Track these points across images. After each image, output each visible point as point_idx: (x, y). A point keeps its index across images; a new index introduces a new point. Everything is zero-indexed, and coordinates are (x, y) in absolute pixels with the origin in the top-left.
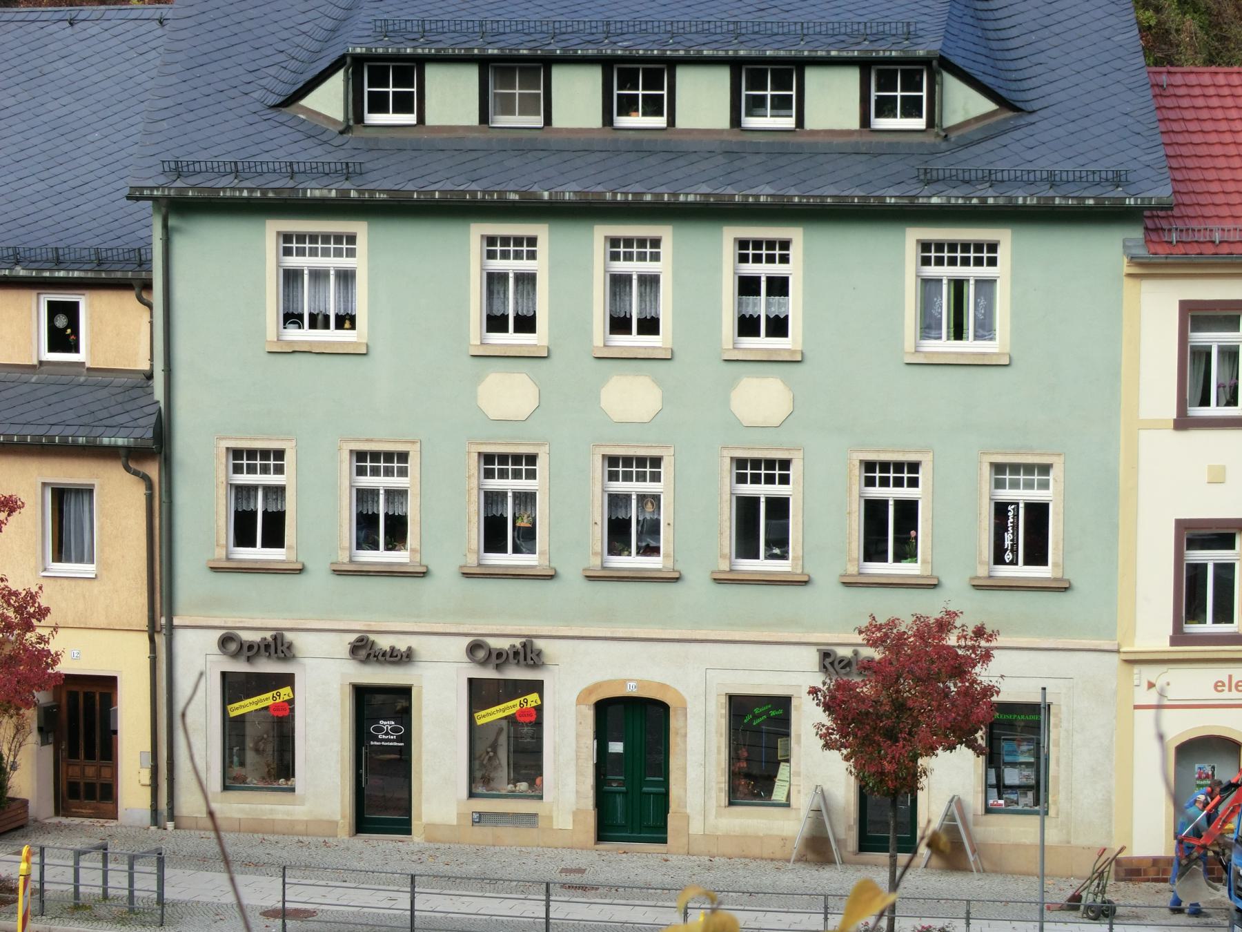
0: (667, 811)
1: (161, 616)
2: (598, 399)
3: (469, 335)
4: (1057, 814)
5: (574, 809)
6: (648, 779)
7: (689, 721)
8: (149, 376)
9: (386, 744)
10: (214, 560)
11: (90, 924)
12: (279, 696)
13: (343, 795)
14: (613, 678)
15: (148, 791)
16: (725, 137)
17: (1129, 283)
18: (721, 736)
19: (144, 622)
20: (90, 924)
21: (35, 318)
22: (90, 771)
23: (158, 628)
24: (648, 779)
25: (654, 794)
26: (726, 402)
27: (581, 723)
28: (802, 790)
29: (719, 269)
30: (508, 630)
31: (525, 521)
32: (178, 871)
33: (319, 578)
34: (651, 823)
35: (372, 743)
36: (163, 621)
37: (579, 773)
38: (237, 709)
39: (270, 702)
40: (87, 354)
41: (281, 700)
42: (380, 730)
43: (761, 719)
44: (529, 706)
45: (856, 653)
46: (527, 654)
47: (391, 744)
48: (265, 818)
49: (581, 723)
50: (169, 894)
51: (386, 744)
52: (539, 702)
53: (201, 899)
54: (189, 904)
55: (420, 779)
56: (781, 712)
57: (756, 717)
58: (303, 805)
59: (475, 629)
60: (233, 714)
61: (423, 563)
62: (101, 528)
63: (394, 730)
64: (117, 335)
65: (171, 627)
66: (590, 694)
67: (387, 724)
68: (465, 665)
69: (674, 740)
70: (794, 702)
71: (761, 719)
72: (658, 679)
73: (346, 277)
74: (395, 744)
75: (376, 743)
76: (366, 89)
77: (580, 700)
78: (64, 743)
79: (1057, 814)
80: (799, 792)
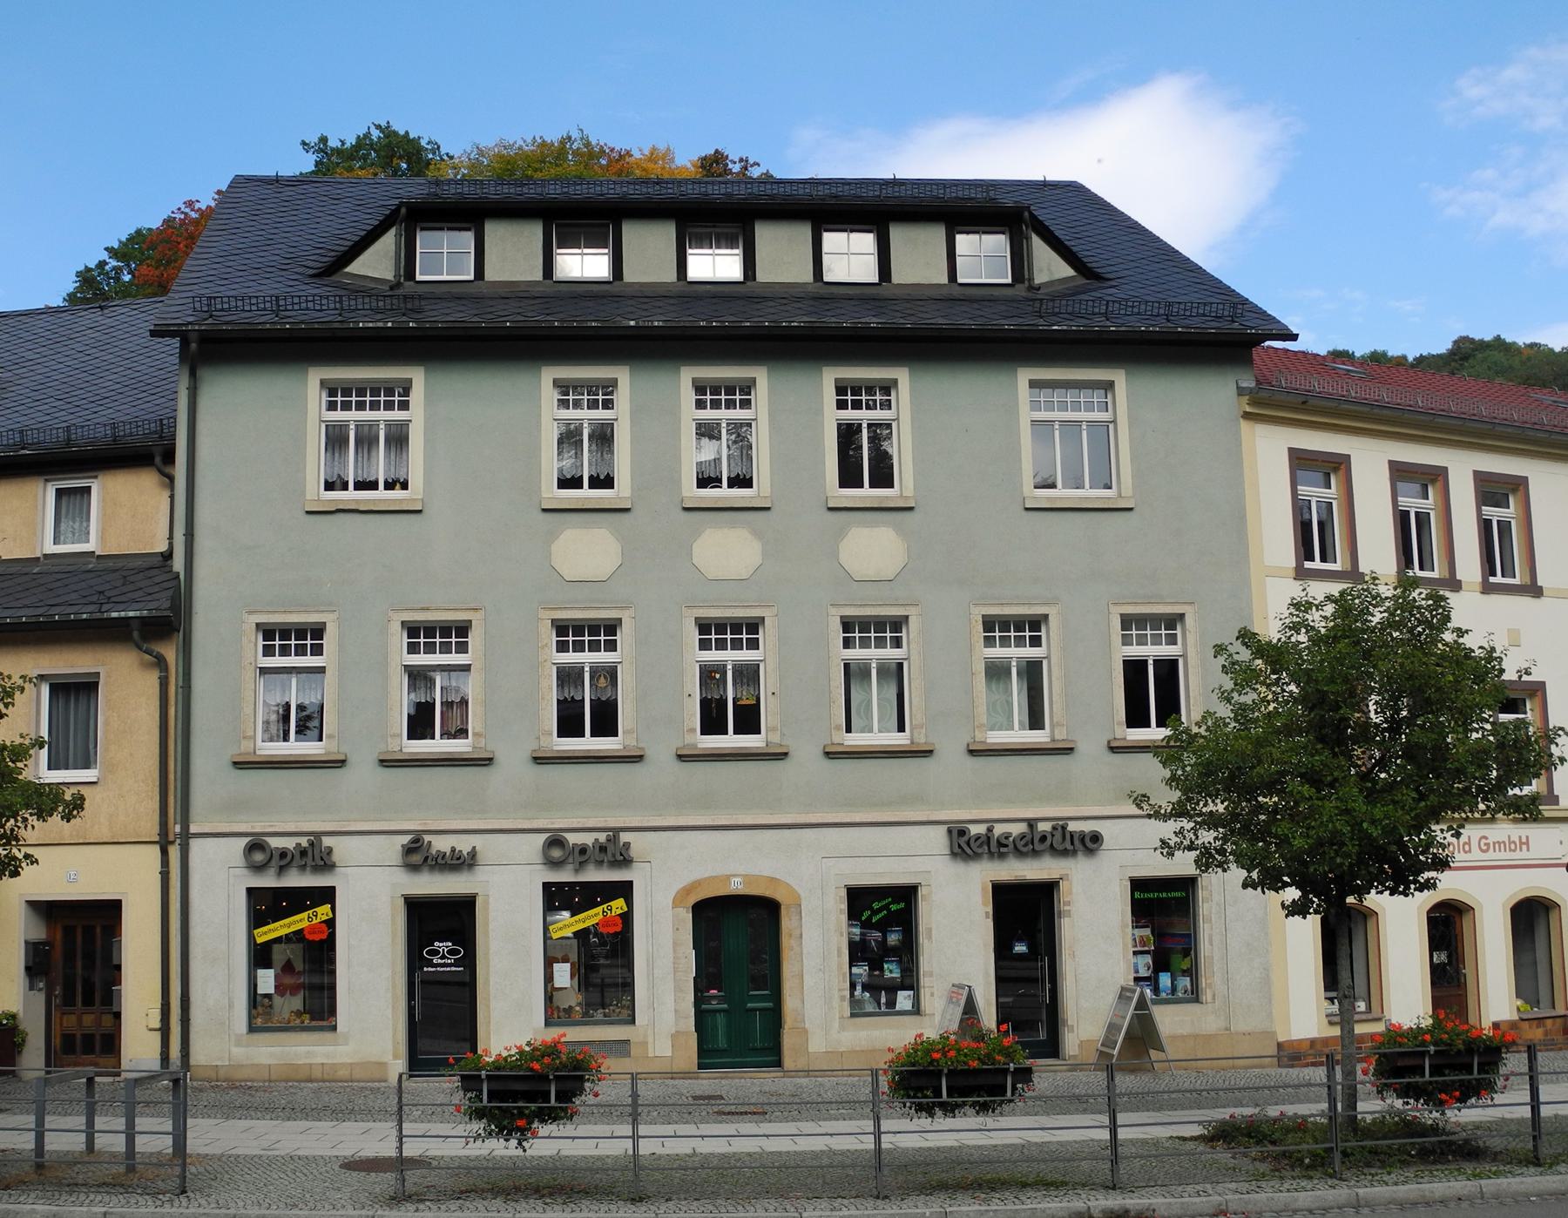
1: (175, 824)
2: (690, 555)
3: (540, 488)
4: (1214, 999)
5: (673, 1031)
6: (751, 993)
8: (168, 556)
9: (442, 969)
10: (240, 755)
11: (82, 1197)
12: (611, 910)
13: (395, 1031)
14: (714, 874)
15: (157, 1036)
16: (810, 289)
17: (1245, 426)
19: (153, 833)
20: (82, 1197)
21: (40, 507)
22: (88, 1020)
23: (171, 838)
24: (751, 993)
25: (761, 1010)
26: (835, 554)
28: (936, 993)
29: (819, 412)
30: (590, 824)
32: (200, 1121)
33: (363, 774)
34: (758, 1045)
35: (425, 969)
36: (178, 829)
37: (678, 989)
38: (265, 934)
39: (305, 924)
40: (97, 543)
41: (319, 920)
42: (435, 953)
43: (880, 916)
44: (613, 914)
45: (990, 830)
46: (614, 851)
47: (448, 969)
49: (678, 929)
50: (194, 1144)
51: (442, 969)
52: (331, 916)
53: (240, 1151)
54: (224, 1159)
56: (902, 905)
57: (875, 912)
58: (347, 1044)
59: (553, 823)
60: (259, 940)
61: (488, 749)
62: (106, 723)
63: (451, 952)
64: (133, 516)
65: (186, 837)
66: (688, 894)
67: (443, 946)
68: (541, 867)
69: (786, 942)
70: (921, 892)
71: (880, 916)
72: (766, 873)
73: (398, 439)
74: (453, 969)
75: (430, 969)
77: (677, 902)
78: (58, 988)
79: (1214, 999)
80: (932, 995)
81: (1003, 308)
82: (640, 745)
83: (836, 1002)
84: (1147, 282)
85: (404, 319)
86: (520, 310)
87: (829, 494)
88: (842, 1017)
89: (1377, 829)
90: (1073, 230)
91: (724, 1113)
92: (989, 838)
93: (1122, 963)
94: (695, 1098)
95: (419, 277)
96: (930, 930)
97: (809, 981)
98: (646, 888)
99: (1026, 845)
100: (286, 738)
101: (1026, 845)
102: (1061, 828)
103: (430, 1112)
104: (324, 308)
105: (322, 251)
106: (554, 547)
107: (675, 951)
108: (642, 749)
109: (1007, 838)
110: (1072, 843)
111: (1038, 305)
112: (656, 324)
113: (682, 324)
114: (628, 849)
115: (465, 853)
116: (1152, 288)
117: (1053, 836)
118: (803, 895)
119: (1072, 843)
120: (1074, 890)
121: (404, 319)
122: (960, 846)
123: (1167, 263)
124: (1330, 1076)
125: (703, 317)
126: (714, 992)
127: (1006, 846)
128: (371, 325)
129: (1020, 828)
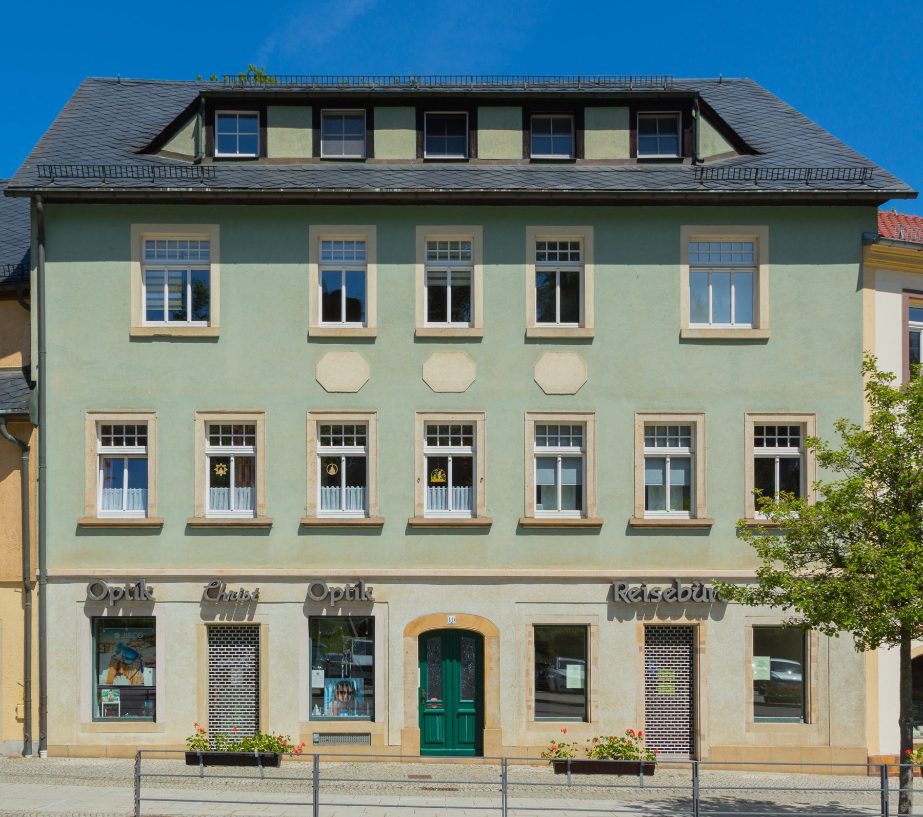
0: (483, 727)
6: (461, 701)
7: (501, 648)
18: (529, 660)
27: (407, 652)
31: (439, 477)
48: (128, 744)
52: (313, 671)
55: (267, 706)
66: (415, 627)
72: (474, 612)
76: (217, 134)
77: (407, 633)
80: (597, 707)
81: (673, 176)
82: (381, 516)
83: (524, 710)
84: (794, 155)
85: (202, 185)
86: (292, 180)
87: (529, 327)
88: (528, 722)
89: (844, 609)
90: (739, 117)
91: (426, 789)
92: (643, 591)
93: (744, 689)
94: (410, 777)
95: (217, 154)
96: (596, 659)
97: (504, 694)
98: (384, 621)
99: (671, 598)
100: (247, 509)
101: (671, 598)
102: (698, 583)
103: (210, 782)
104: (140, 176)
105: (147, 135)
106: (318, 365)
107: (405, 668)
108: (383, 519)
109: (657, 592)
110: (708, 597)
111: (700, 175)
112: (396, 190)
113: (416, 190)
114: (371, 593)
115: (250, 593)
116: (798, 159)
117: (693, 591)
118: (501, 630)
119: (708, 597)
120: (709, 633)
121: (202, 185)
122: (620, 597)
123: (814, 139)
124: (883, 784)
125: (433, 185)
126: (434, 700)
127: (656, 597)
128: (176, 190)
129: (665, 587)
